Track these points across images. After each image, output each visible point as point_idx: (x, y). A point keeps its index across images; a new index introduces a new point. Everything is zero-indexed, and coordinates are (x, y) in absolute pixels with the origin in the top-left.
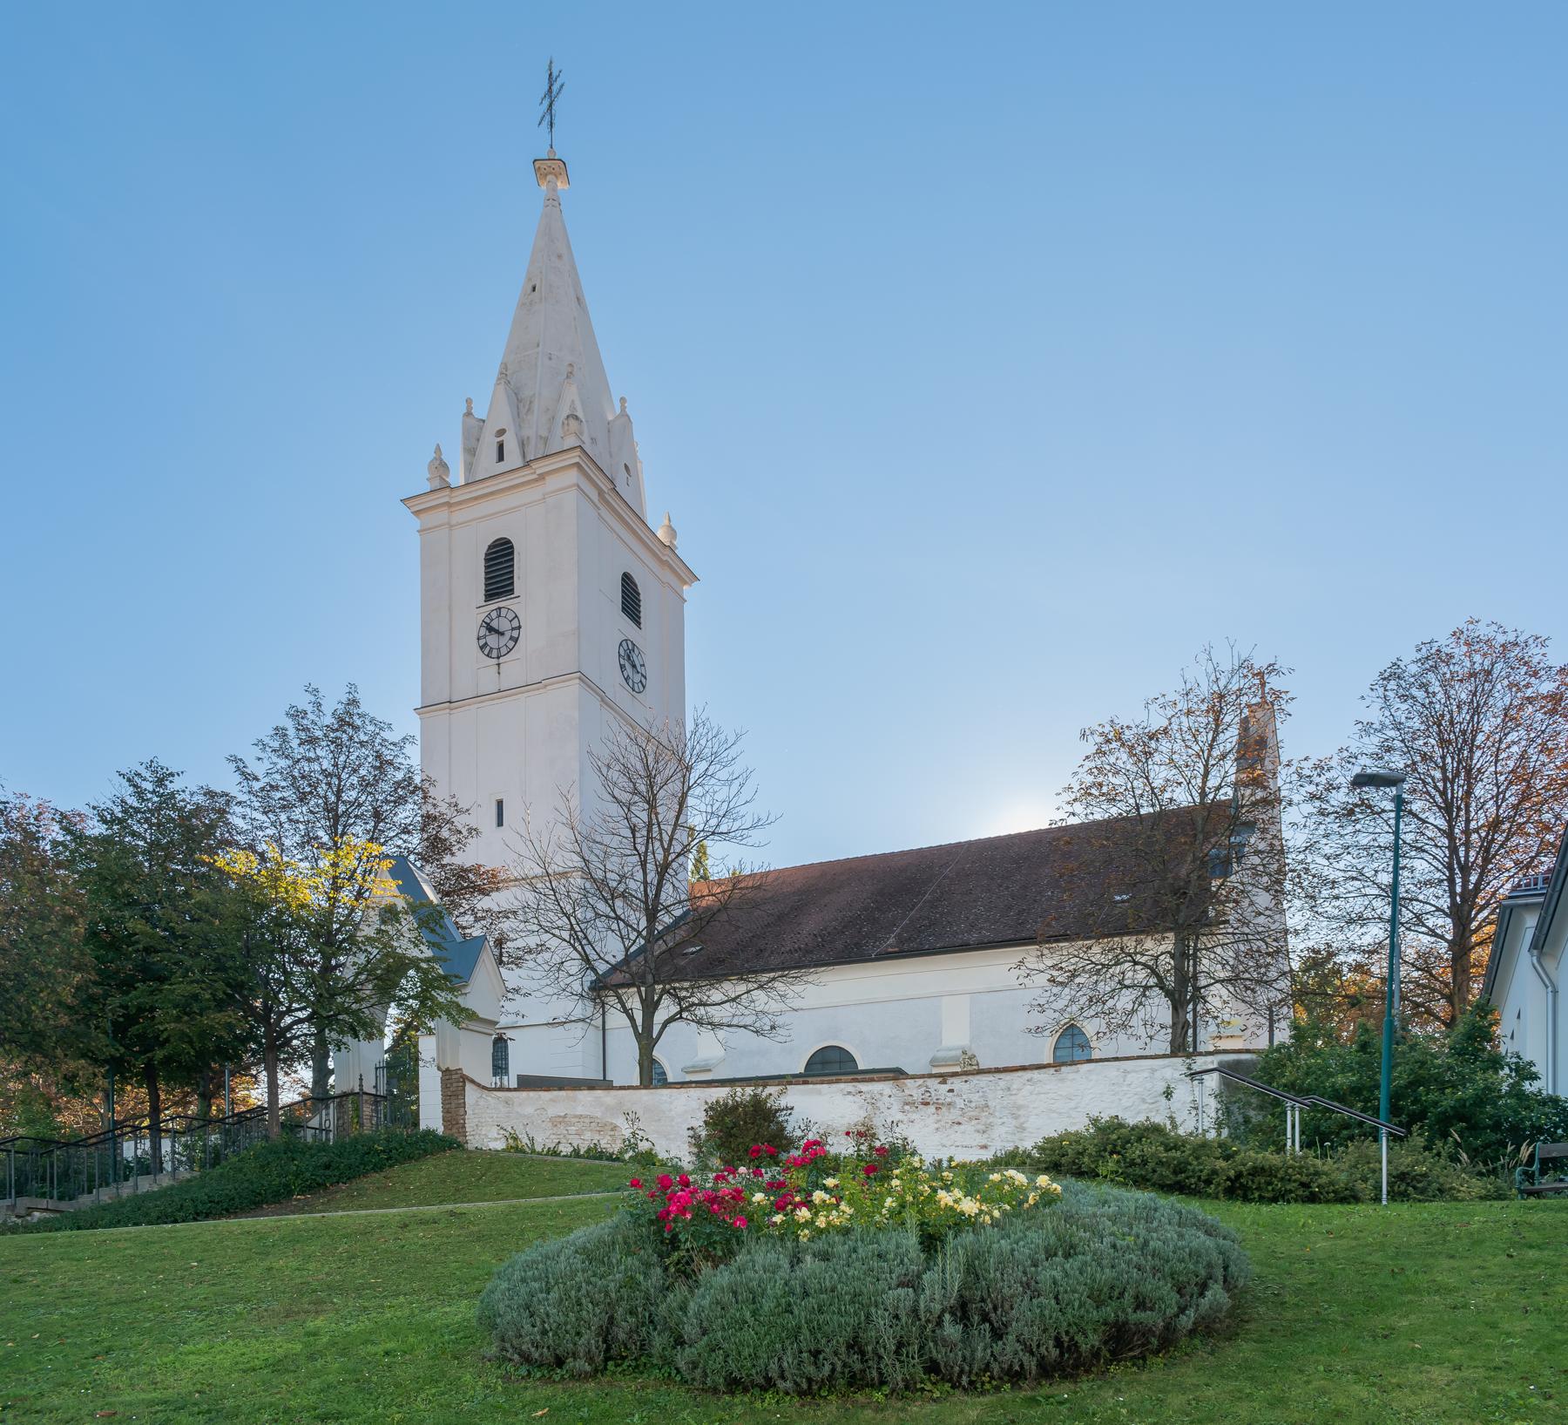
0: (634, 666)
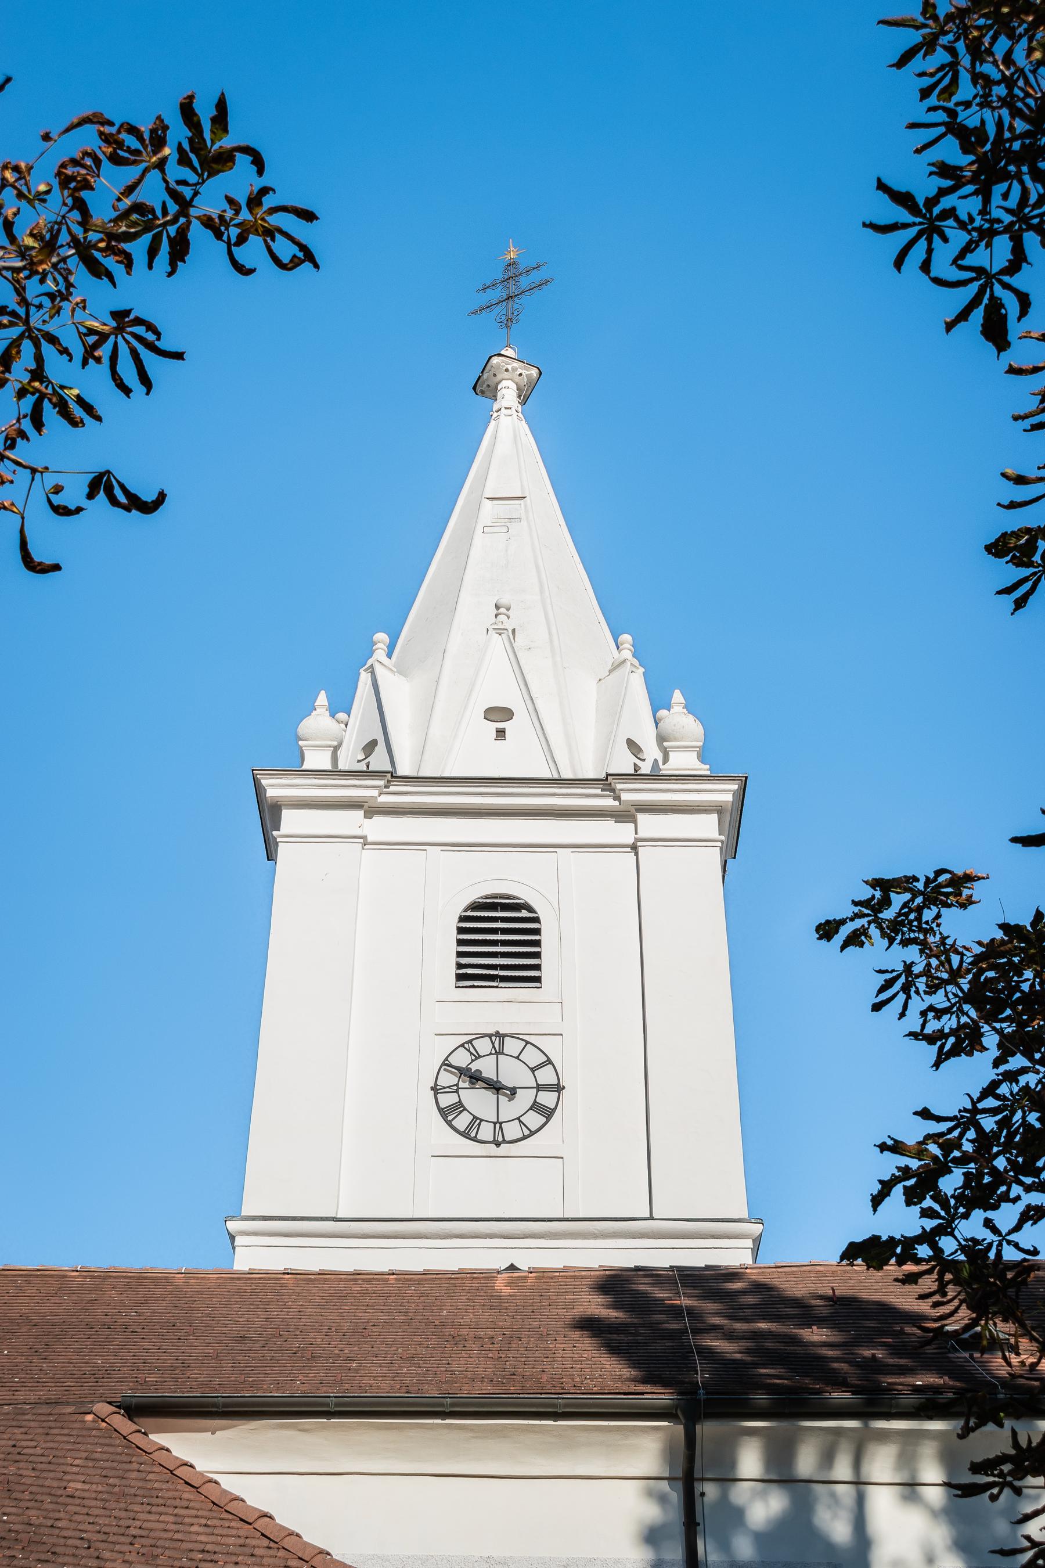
0: (496, 1087)
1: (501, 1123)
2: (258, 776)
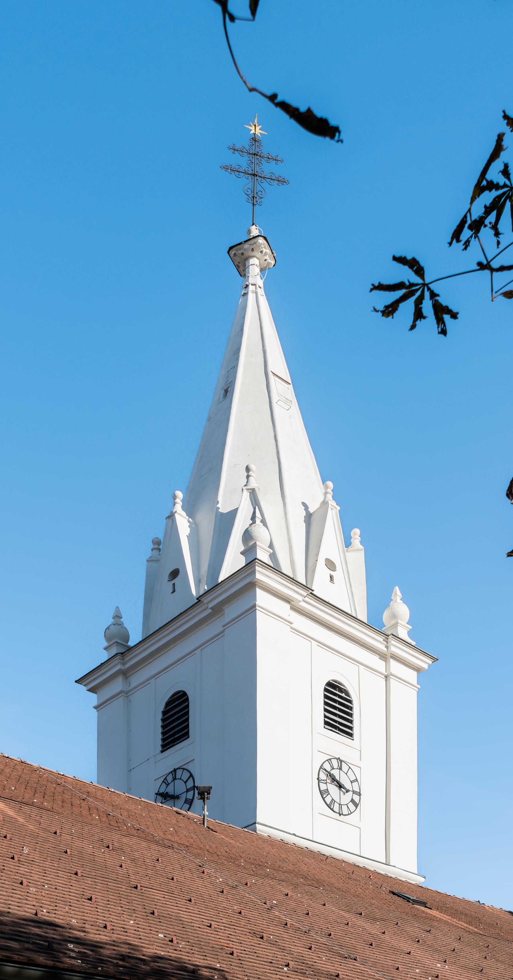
0: (340, 786)
1: (341, 805)
2: (256, 563)
